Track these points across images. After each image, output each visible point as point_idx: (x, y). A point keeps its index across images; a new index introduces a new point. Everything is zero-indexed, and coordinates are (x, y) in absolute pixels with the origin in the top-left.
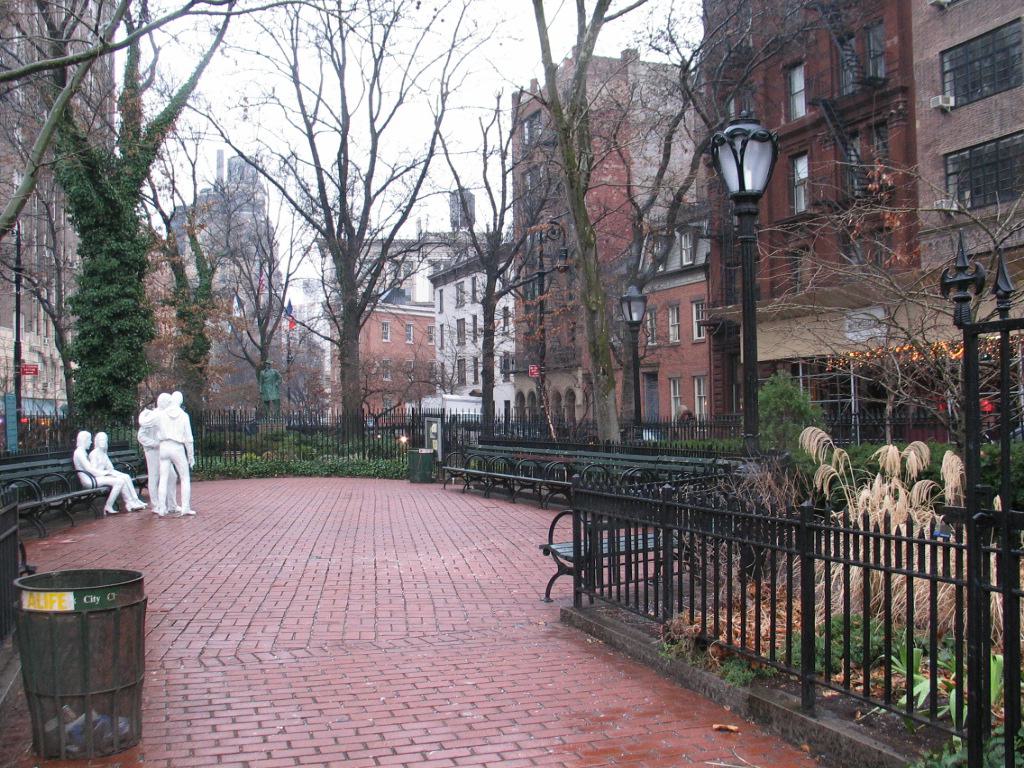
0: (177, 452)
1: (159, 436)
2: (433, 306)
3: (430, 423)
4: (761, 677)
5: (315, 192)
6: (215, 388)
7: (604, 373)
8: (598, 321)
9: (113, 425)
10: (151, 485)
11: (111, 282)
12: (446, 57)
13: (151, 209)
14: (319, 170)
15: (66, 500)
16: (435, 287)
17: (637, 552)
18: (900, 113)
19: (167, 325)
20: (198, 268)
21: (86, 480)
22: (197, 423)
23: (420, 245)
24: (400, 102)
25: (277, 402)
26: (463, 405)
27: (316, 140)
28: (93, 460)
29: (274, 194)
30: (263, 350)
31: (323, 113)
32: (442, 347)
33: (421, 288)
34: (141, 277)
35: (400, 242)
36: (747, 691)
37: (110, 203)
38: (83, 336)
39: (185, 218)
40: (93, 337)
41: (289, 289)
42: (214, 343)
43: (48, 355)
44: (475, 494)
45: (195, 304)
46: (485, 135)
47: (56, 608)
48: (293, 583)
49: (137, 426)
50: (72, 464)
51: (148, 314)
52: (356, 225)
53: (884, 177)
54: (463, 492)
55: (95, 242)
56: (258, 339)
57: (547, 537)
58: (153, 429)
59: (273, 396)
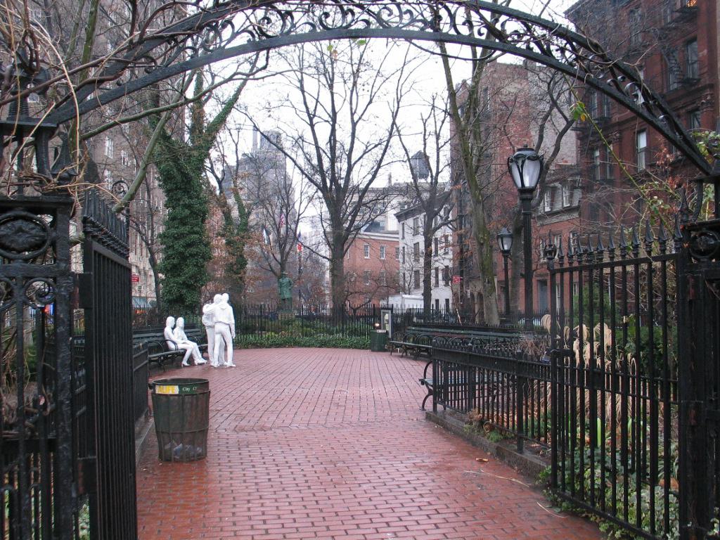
0: (225, 329)
1: (215, 320)
2: (398, 234)
3: (384, 314)
4: (506, 438)
5: (315, 162)
6: (250, 290)
7: (489, 282)
8: (485, 249)
9: (186, 314)
10: (209, 350)
11: (185, 224)
12: (400, 72)
13: (209, 174)
14: (318, 148)
15: (160, 357)
16: (399, 221)
17: (459, 385)
18: (708, 102)
19: (219, 250)
20: (239, 212)
21: (172, 346)
22: (237, 313)
23: (386, 193)
24: (370, 102)
25: (290, 299)
26: (412, 301)
27: (315, 128)
28: (176, 334)
29: (289, 163)
30: (282, 264)
31: (320, 111)
32: (404, 263)
33: (392, 223)
34: (203, 221)
35: (373, 191)
36: (497, 444)
37: (185, 175)
38: (168, 258)
39: (231, 174)
40: (174, 259)
41: (300, 224)
42: (249, 261)
43: (142, 268)
44: (409, 358)
45: (239, 233)
46: (425, 124)
47: (171, 393)
48: (287, 400)
49: (201, 314)
50: (163, 336)
51: (207, 244)
52: (342, 182)
53: (668, 156)
54: (402, 357)
55: (176, 200)
56: (278, 257)
57: (423, 375)
58: (211, 316)
59: (287, 296)
